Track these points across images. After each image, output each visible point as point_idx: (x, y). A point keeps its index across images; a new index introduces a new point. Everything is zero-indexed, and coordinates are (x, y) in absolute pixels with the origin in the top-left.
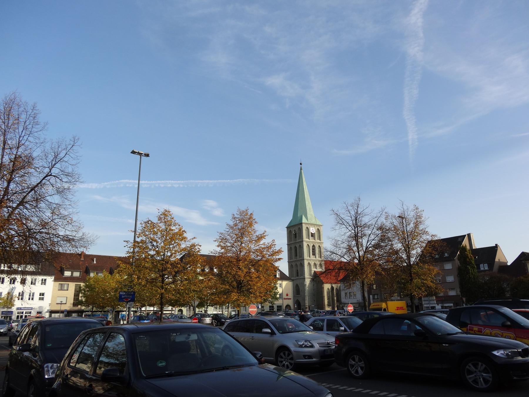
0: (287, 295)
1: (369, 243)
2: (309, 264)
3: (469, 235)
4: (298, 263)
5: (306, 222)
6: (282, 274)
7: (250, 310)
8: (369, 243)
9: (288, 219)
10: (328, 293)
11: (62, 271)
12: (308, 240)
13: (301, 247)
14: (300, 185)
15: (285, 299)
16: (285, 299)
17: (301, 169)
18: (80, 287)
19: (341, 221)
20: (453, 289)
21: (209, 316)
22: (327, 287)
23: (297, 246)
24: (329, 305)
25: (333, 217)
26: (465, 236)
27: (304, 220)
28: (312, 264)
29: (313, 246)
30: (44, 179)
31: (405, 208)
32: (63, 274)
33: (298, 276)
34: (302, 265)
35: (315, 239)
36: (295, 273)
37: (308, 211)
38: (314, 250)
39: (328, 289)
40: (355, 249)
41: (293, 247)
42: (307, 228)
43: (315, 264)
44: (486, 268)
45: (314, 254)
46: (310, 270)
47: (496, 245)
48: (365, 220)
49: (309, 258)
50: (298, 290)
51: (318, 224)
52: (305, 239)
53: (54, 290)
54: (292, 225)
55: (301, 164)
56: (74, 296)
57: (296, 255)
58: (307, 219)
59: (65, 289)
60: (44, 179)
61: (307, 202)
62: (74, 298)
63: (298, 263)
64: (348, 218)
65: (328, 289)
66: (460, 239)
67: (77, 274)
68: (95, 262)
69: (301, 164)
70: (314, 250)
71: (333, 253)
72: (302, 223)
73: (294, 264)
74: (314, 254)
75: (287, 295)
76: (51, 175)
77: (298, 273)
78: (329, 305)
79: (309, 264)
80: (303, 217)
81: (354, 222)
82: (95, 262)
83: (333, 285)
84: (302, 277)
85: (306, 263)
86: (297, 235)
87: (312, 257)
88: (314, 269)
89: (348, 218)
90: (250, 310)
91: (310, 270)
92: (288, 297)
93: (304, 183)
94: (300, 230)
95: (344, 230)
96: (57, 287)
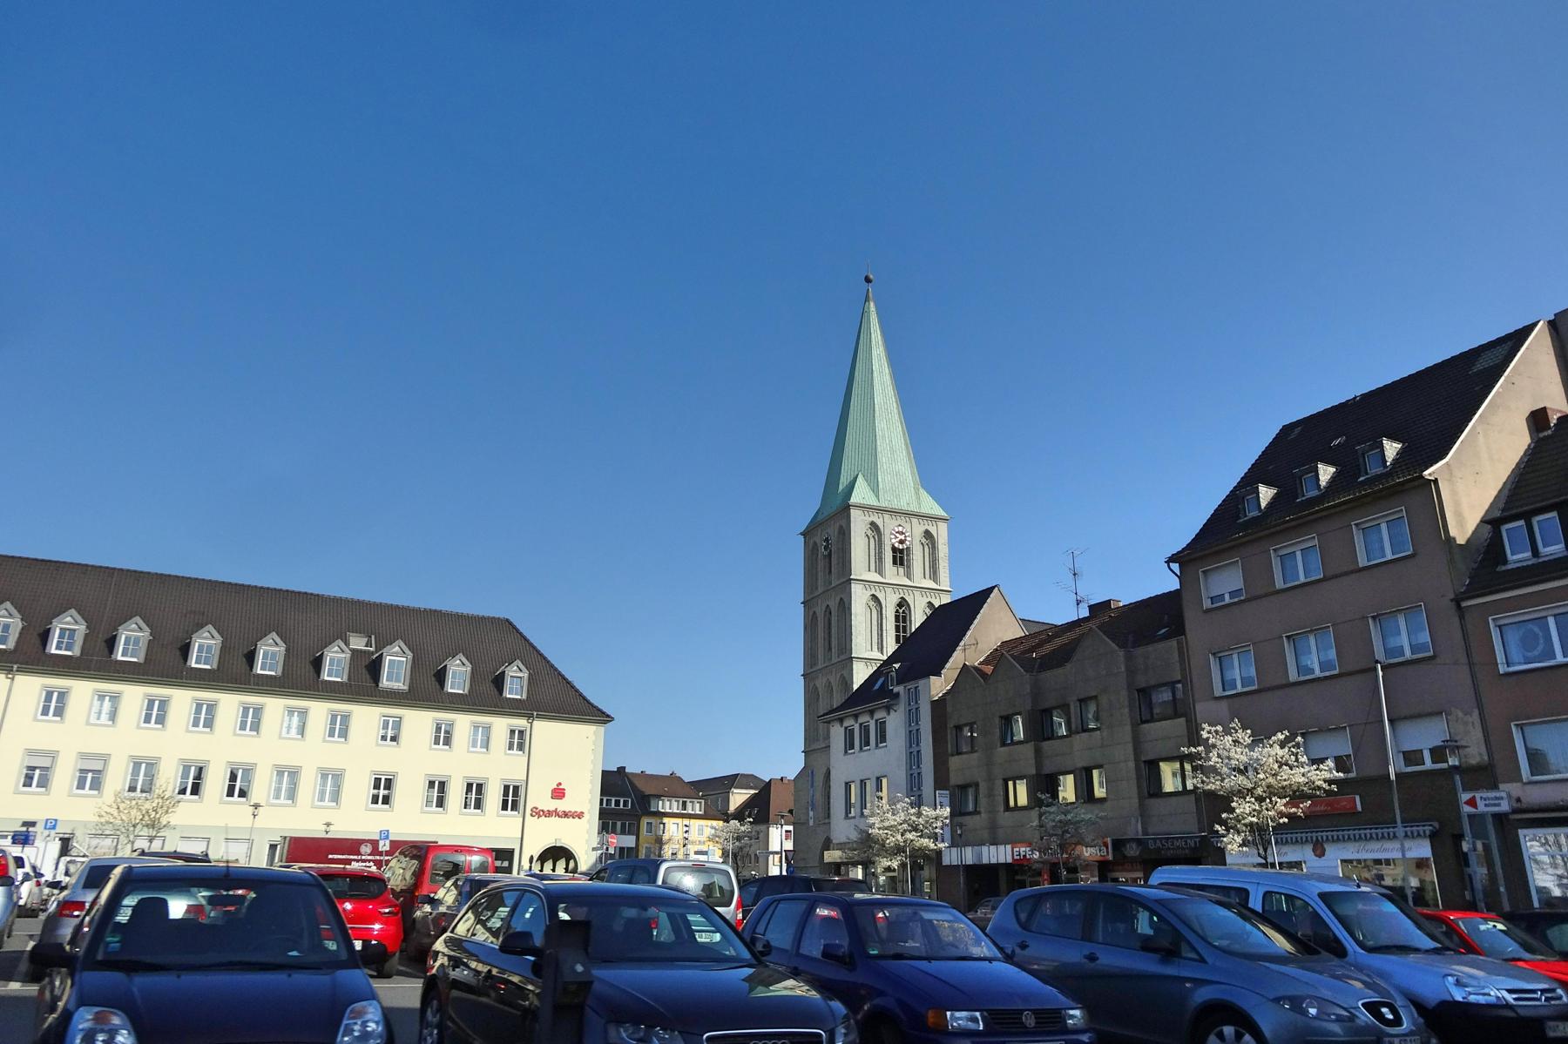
0: (558, 793)
5: (871, 500)
15: (538, 813)
16: (538, 813)
29: (902, 603)
35: (909, 575)
41: (820, 611)
42: (874, 525)
58: (875, 489)
59: (971, 807)
69: (868, 280)
75: (558, 793)
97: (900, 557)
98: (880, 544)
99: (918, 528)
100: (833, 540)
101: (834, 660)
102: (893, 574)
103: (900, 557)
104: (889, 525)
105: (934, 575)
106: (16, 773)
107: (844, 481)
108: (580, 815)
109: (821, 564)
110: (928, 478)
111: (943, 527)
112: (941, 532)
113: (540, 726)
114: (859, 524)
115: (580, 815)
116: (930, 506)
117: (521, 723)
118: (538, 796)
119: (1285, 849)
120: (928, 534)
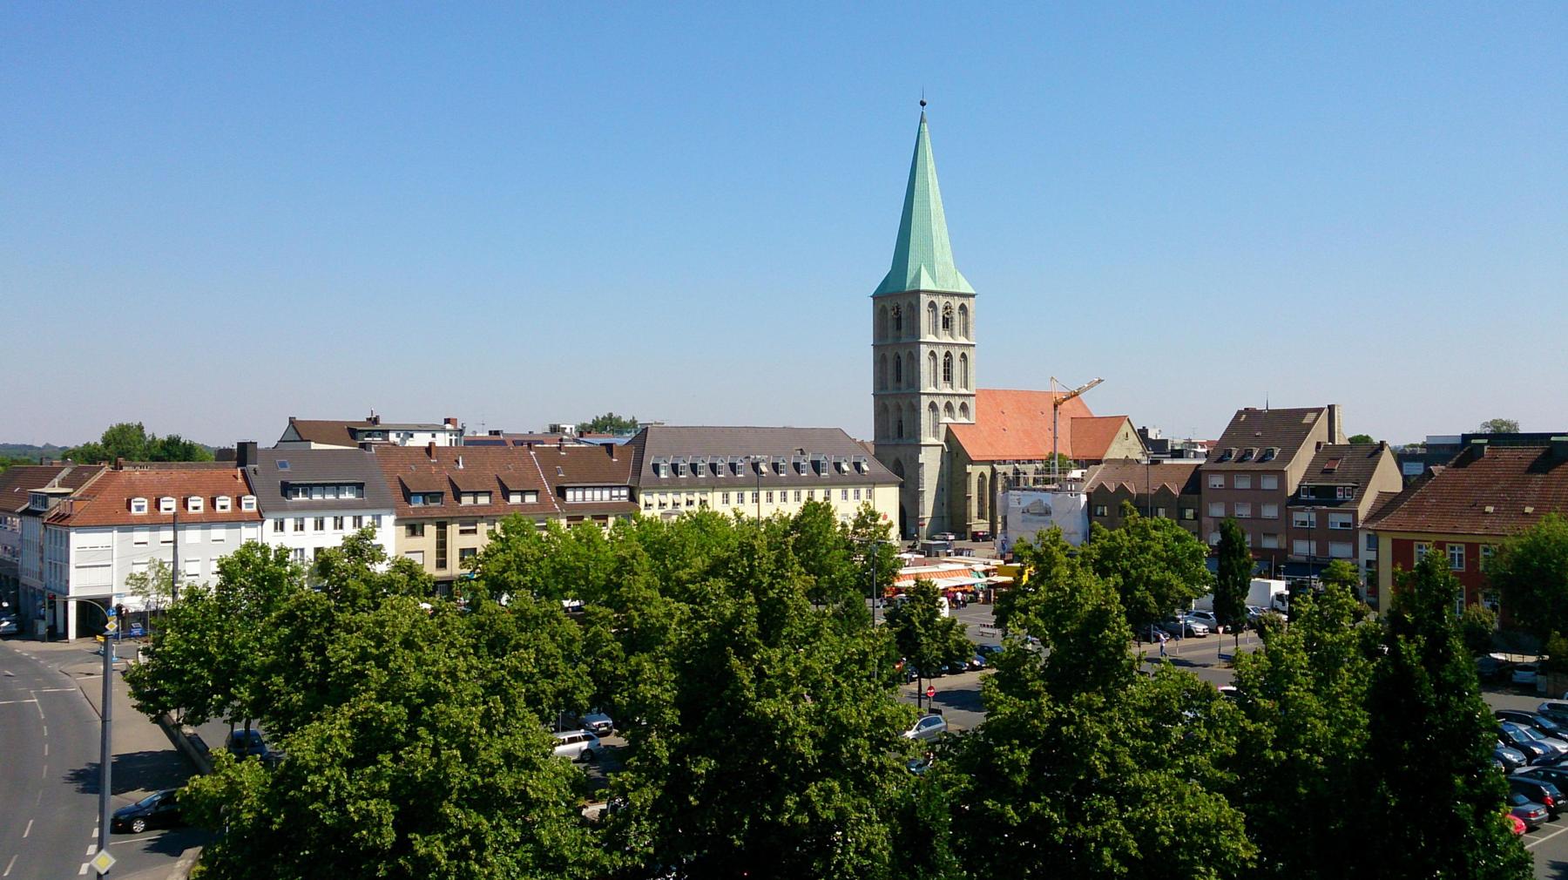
2: (932, 353)
3: (1331, 408)
17: (922, 120)
18: (373, 559)
20: (1274, 535)
21: (626, 800)
23: (903, 354)
26: (1319, 411)
29: (948, 354)
33: (900, 435)
36: (893, 431)
37: (937, 254)
38: (948, 365)
39: (982, 475)
41: (890, 355)
44: (1064, 729)
46: (937, 425)
51: (962, 291)
54: (889, 290)
55: (923, 104)
57: (899, 379)
58: (933, 277)
61: (935, 227)
63: (904, 403)
65: (982, 475)
70: (948, 365)
73: (890, 403)
74: (948, 377)
77: (900, 428)
78: (981, 515)
79: (932, 353)
80: (924, 272)
85: (925, 402)
86: (904, 323)
91: (937, 425)
93: (931, 166)
99: (956, 303)
100: (903, 309)
104: (941, 302)
110: (962, 265)
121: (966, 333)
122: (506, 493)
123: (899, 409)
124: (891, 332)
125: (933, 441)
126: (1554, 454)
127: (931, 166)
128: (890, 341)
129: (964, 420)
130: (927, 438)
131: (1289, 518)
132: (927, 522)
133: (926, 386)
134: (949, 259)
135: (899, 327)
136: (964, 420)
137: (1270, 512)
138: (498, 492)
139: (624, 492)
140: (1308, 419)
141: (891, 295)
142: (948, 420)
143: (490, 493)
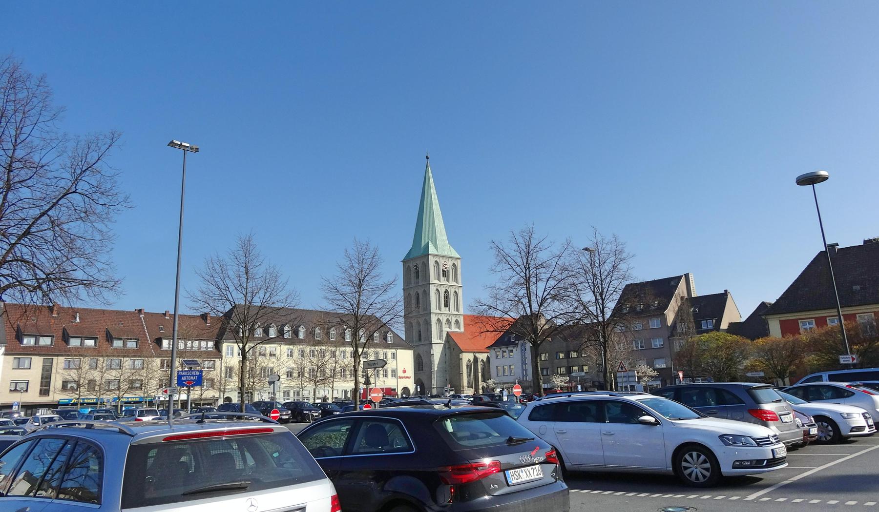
0: (404, 371)
1: (546, 293)
2: (439, 320)
3: (687, 276)
4: (421, 321)
5: (435, 252)
6: (396, 336)
7: (373, 395)
8: (546, 293)
9: (406, 246)
10: (468, 366)
11: (19, 337)
12: (437, 282)
13: (427, 294)
14: (426, 191)
15: (400, 377)
16: (400, 377)
19: (503, 258)
22: (467, 357)
23: (420, 292)
24: (469, 386)
25: (494, 252)
26: (680, 278)
27: (432, 250)
28: (444, 319)
29: (446, 291)
30: (62, 197)
31: (599, 238)
32: (21, 342)
33: (420, 339)
34: (428, 323)
35: (448, 281)
38: (447, 298)
39: (469, 360)
40: (525, 301)
41: (413, 293)
42: (436, 262)
43: (448, 321)
45: (447, 305)
46: (441, 331)
47: (726, 291)
48: (542, 256)
49: (438, 311)
50: (421, 364)
52: (433, 280)
53: (4, 368)
54: (411, 257)
55: (427, 158)
56: (42, 378)
58: (436, 248)
59: (26, 366)
60: (62, 197)
62: (42, 382)
64: (511, 249)
65: (469, 360)
66: (673, 283)
67: (45, 341)
68: (78, 320)
69: (427, 158)
71: (491, 307)
72: (428, 255)
74: (447, 305)
75: (404, 371)
76: (74, 192)
77: (420, 335)
78: (469, 386)
79: (439, 320)
80: (431, 245)
81: (525, 261)
82: (78, 320)
83: (477, 355)
84: (427, 342)
85: (434, 319)
87: (444, 310)
88: (446, 329)
89: (511, 249)
90: (373, 395)
91: (441, 331)
92: (406, 375)
93: (433, 189)
94: (426, 265)
95: (510, 273)
96: (11, 364)
97: (445, 274)
98: (439, 269)
99: (450, 263)
100: (420, 266)
101: (421, 313)
102: (443, 281)
103: (445, 274)
104: (442, 262)
105: (456, 281)
106: (8, 387)
107: (423, 243)
108: (409, 378)
109: (413, 275)
110: (452, 243)
111: (459, 261)
112: (459, 264)
113: (398, 351)
114: (432, 260)
115: (409, 378)
116: (455, 254)
117: (394, 351)
118: (400, 374)
119: (846, 309)
120: (454, 265)
121: (456, 281)
122: (110, 338)
123: (419, 324)
124: (413, 280)
125: (440, 341)
126: (877, 251)
127: (433, 189)
128: (413, 285)
129: (457, 330)
130: (435, 339)
131: (671, 346)
132: (436, 369)
133: (434, 308)
134: (445, 238)
135: (418, 277)
136: (457, 330)
137: (657, 343)
138: (102, 338)
139: (211, 344)
140: (673, 283)
141: (412, 259)
142: (449, 330)
143: (95, 339)
